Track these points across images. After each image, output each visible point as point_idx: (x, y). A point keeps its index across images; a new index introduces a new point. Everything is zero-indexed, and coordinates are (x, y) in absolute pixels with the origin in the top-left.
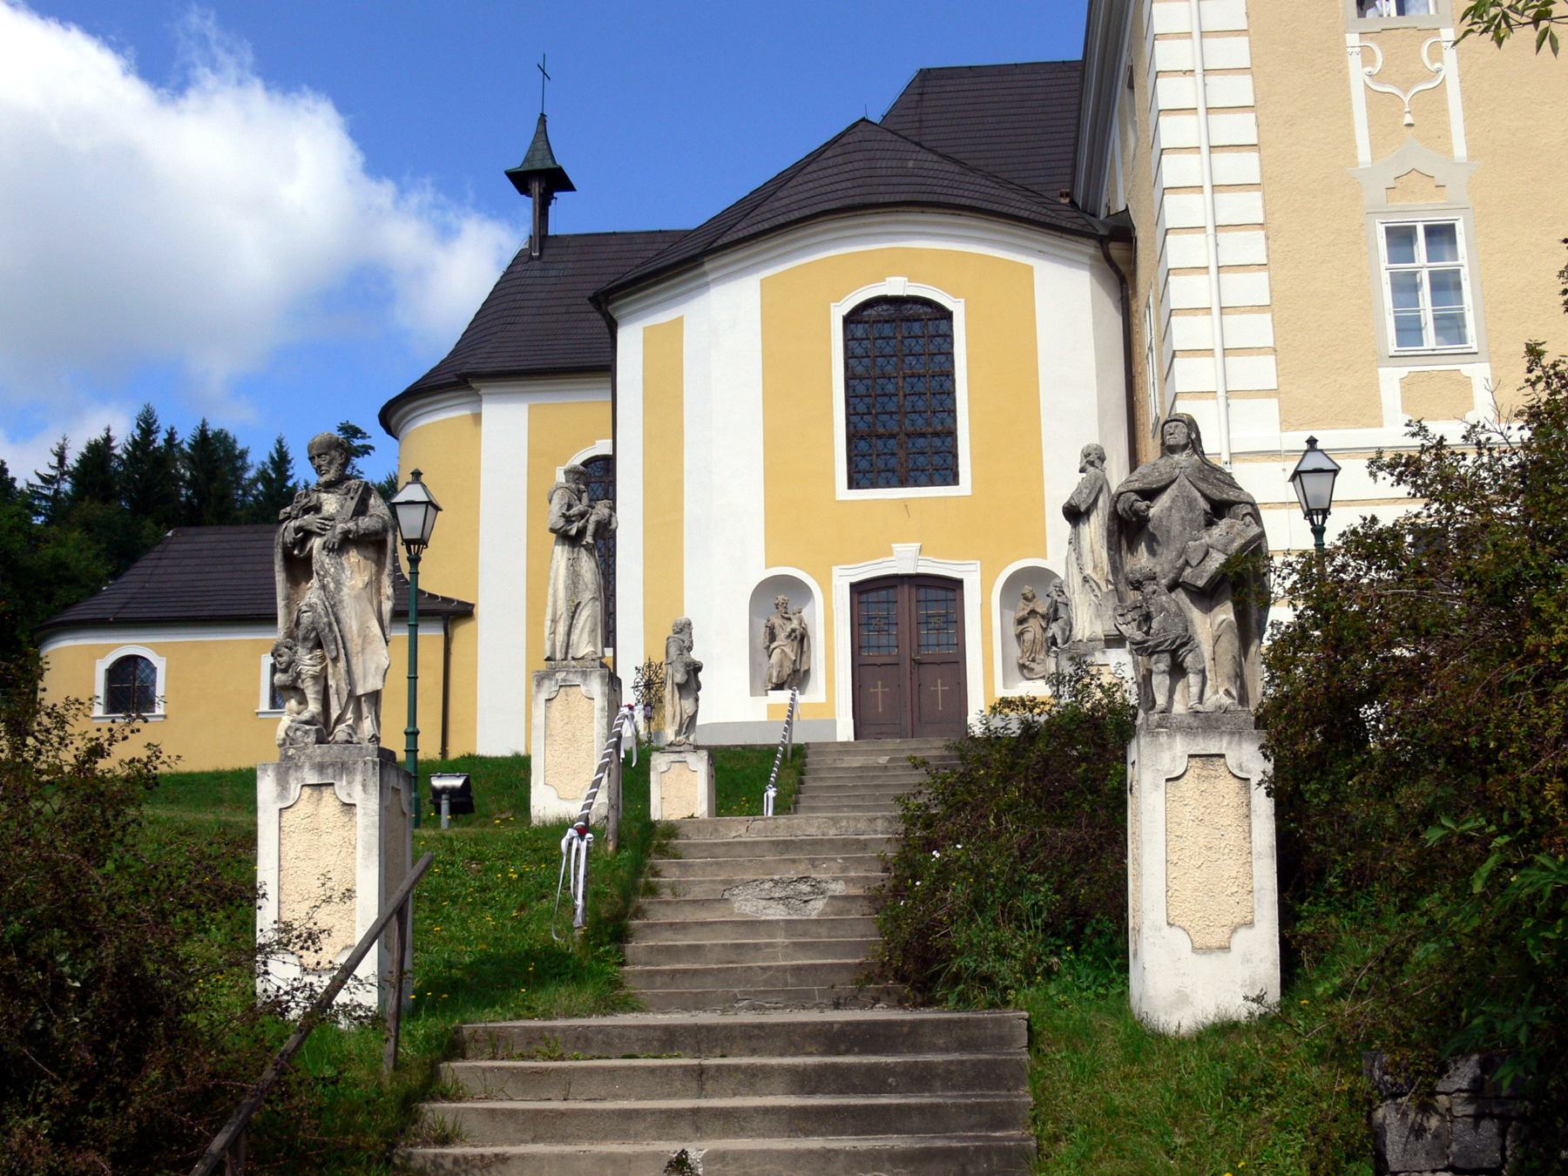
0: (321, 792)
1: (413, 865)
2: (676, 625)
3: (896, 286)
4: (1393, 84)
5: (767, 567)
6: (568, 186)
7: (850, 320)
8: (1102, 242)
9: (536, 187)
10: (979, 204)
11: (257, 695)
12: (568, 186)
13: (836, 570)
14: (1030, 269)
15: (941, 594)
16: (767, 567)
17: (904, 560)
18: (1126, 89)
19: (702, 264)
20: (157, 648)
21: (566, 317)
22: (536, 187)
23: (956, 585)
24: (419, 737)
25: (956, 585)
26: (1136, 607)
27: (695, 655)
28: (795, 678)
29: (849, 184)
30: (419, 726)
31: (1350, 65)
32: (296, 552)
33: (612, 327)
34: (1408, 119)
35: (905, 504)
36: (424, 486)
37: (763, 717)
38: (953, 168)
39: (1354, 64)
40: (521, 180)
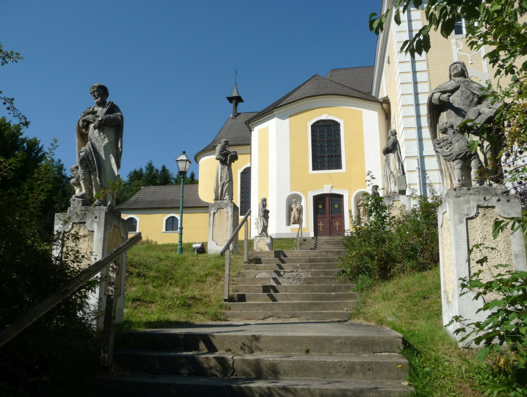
0: (80, 226)
1: (119, 258)
2: (262, 200)
3: (324, 117)
4: (466, 52)
5: (291, 191)
6: (242, 101)
7: (313, 126)
8: (381, 103)
9: (234, 101)
10: (347, 94)
11: (162, 227)
12: (242, 101)
13: (309, 192)
14: (361, 112)
15: (338, 199)
16: (291, 191)
17: (326, 190)
18: (387, 63)
19: (273, 112)
20: (138, 217)
21: (241, 132)
22: (234, 101)
23: (341, 197)
24: (183, 230)
25: (341, 197)
26: (444, 140)
27: (267, 208)
28: (298, 221)
29: (312, 90)
30: (183, 226)
31: (453, 48)
32: (83, 130)
33: (250, 130)
34: (470, 62)
35: (328, 174)
36: (186, 156)
37: (289, 232)
38: (340, 86)
39: (454, 47)
40: (230, 99)
